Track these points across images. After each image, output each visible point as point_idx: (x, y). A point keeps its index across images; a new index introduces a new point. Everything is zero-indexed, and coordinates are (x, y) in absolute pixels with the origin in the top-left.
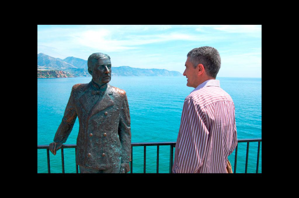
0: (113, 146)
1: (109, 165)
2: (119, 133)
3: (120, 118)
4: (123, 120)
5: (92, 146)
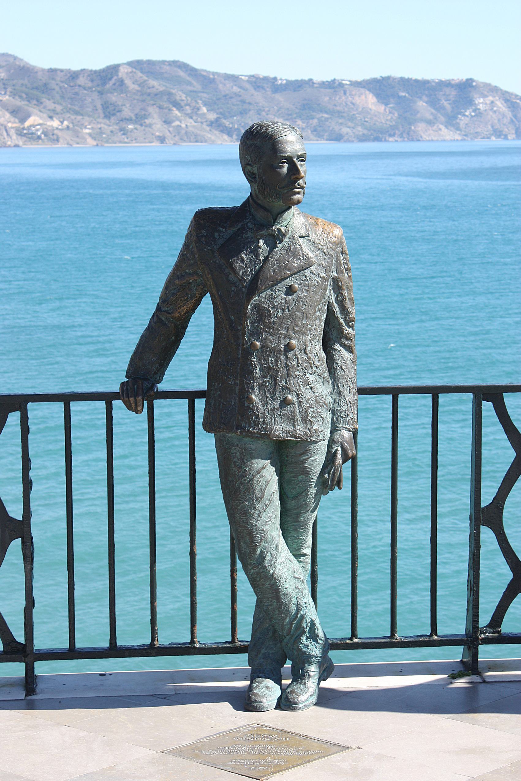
0: (311, 378)
1: (300, 429)
2: (327, 346)
3: (329, 302)
4: (337, 309)
5: (258, 375)
